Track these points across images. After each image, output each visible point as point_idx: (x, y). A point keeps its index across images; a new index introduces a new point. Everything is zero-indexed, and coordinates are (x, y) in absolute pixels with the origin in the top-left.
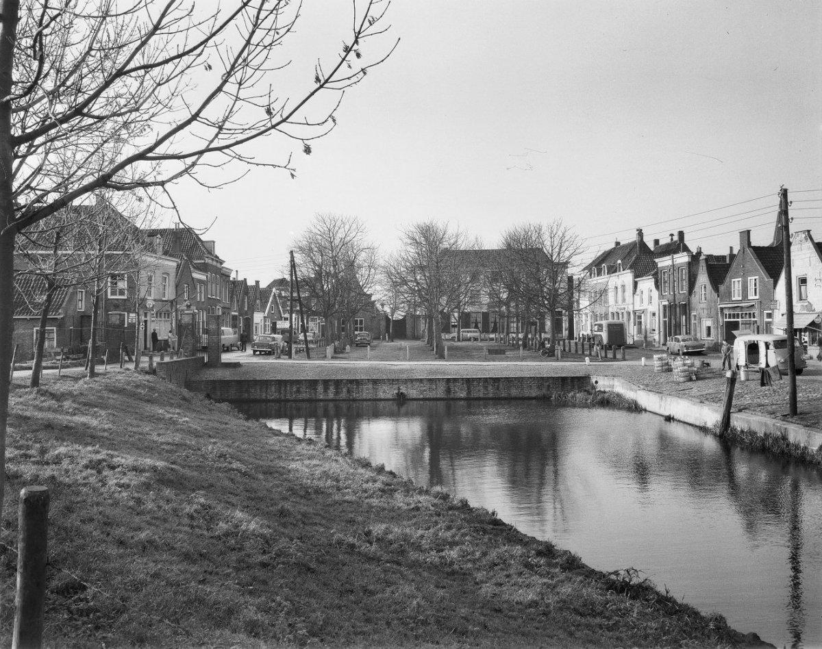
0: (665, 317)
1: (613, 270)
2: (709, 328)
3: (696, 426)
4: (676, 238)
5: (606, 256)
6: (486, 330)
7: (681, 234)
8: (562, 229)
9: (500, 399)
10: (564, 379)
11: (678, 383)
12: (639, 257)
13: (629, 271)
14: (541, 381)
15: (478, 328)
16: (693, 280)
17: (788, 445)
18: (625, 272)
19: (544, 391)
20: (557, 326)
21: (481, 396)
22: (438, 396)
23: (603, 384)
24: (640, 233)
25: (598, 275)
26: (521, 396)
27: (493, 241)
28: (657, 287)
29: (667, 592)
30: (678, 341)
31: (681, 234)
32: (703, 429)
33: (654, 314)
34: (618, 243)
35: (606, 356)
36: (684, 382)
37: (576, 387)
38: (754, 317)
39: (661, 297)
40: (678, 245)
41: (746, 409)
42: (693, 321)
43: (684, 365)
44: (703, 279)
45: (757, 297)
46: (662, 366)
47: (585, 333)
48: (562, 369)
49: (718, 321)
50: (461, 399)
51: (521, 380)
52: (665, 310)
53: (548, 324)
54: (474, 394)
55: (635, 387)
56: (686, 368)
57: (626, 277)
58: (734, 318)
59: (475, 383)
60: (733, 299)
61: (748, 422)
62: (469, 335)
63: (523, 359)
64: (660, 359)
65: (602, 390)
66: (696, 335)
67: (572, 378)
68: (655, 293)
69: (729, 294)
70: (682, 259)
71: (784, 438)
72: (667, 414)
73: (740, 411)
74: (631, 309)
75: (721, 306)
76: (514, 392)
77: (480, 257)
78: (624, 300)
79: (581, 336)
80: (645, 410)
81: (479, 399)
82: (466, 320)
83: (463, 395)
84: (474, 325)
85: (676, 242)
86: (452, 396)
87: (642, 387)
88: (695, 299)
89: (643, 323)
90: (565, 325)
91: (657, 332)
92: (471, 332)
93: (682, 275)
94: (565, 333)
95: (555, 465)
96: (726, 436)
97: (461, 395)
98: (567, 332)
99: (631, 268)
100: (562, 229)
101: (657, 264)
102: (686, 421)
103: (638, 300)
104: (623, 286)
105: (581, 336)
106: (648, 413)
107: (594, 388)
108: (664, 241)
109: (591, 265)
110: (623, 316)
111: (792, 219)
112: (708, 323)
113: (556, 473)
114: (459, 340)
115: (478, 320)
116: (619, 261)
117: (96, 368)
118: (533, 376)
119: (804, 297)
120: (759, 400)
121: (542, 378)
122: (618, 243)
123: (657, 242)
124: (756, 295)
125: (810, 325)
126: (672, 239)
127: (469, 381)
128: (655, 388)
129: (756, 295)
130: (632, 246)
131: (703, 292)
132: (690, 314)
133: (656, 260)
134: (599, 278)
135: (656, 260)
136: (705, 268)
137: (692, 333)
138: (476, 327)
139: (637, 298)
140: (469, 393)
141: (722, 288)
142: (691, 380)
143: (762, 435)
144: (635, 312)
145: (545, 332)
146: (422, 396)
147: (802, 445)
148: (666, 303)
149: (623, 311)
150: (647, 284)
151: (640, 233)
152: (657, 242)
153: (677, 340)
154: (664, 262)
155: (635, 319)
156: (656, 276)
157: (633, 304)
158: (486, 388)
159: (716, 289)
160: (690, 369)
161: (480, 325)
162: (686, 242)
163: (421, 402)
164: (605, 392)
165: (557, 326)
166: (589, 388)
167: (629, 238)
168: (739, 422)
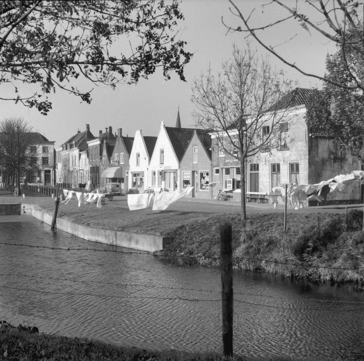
34: (79, 132)
44: (105, 153)
57: (76, 151)
101: (87, 144)
126: (107, 131)
133: (88, 142)
135: (88, 142)
150: (84, 156)
152: (101, 132)
157: (79, 166)
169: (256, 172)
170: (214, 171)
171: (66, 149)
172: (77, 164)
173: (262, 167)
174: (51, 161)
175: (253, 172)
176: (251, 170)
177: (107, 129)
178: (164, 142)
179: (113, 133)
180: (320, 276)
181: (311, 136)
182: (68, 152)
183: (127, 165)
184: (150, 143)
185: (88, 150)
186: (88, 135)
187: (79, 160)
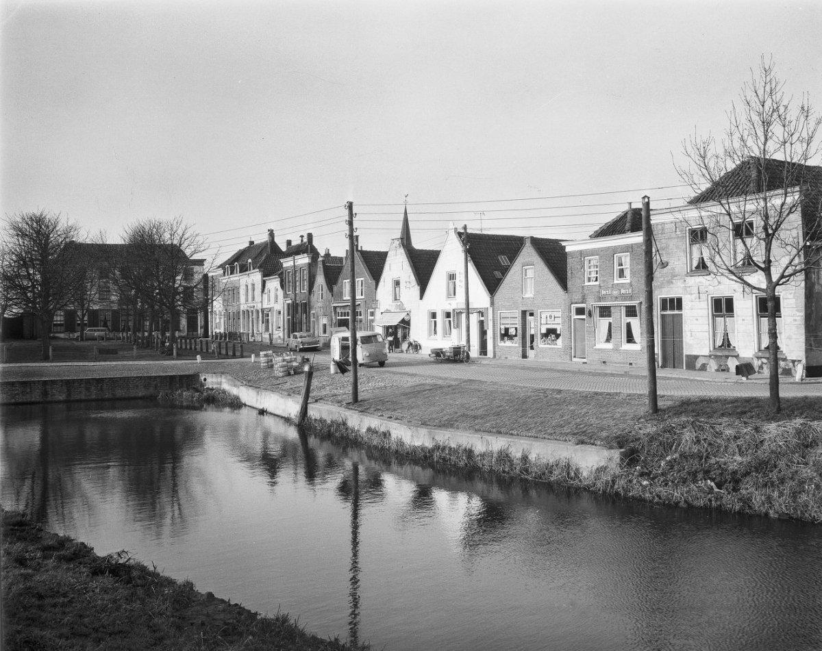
0: (288, 315)
1: (244, 269)
2: (325, 325)
3: (282, 417)
4: (305, 240)
5: (239, 256)
6: (116, 329)
7: (310, 236)
8: (183, 227)
9: (103, 400)
10: (172, 378)
11: (277, 378)
12: (265, 258)
13: (258, 270)
14: (148, 381)
15: (107, 327)
16: (312, 280)
17: (347, 429)
18: (254, 271)
19: (151, 390)
20: (192, 325)
21: (83, 397)
22: (33, 400)
23: (212, 381)
24: (271, 233)
25: (231, 274)
26: (127, 396)
27: (116, 235)
28: (282, 286)
29: (155, 568)
30: (296, 338)
31: (310, 236)
32: (287, 420)
33: (280, 313)
34: (252, 243)
35: (227, 354)
36: (283, 377)
37: (185, 385)
38: (361, 315)
39: (286, 296)
40: (307, 247)
41: (321, 399)
42: (312, 319)
43: (284, 360)
44: (320, 280)
45: (363, 297)
46: (268, 362)
47: (218, 331)
48: (172, 367)
49: (332, 320)
50: (59, 402)
51: (126, 380)
52: (288, 308)
53: (184, 322)
54: (75, 397)
55: (239, 383)
56: (285, 363)
57: (256, 276)
58: (672, 308)
59: (76, 384)
60: (345, 299)
61: (319, 411)
62: (96, 334)
63: (140, 358)
64: (266, 356)
65: (210, 387)
66: (314, 333)
67: (181, 376)
68: (280, 293)
69: (341, 294)
70: (303, 260)
71: (344, 424)
72: (261, 407)
73: (316, 401)
74: (259, 307)
75: (334, 305)
76: (120, 393)
77: (102, 252)
78: (253, 299)
79: (214, 334)
80: (245, 405)
81: (80, 401)
82: (95, 319)
83: (62, 397)
84: (102, 323)
85: (305, 243)
86: (49, 398)
87: (245, 382)
88: (314, 298)
89: (270, 321)
90: (200, 321)
91: (282, 329)
92: (98, 330)
93: (303, 275)
94: (200, 331)
95: (174, 468)
96: (304, 425)
97: (61, 398)
98: (203, 330)
99: (260, 267)
100: (183, 227)
101: (282, 264)
102: (275, 413)
103: (264, 297)
104: (253, 285)
105: (214, 334)
106: (247, 407)
107: (202, 385)
108: (296, 242)
109: (226, 263)
110: (253, 314)
111: (356, 229)
112: (324, 321)
113: (174, 476)
114: (82, 340)
115: (108, 318)
116: (250, 261)
117: (769, 394)
118: (141, 375)
119: (398, 298)
120: (335, 391)
121: (150, 378)
122: (252, 243)
123: (289, 242)
124: (362, 295)
125: (401, 322)
126: (302, 241)
127: (69, 384)
128: (254, 384)
129: (362, 295)
130: (263, 247)
131: (321, 292)
132: (309, 312)
133: (282, 260)
134: (231, 276)
135: (282, 260)
136: (322, 269)
137: (312, 332)
138: (105, 325)
139: (265, 296)
140: (69, 395)
141: (335, 288)
142: (289, 374)
143: (329, 422)
144: (263, 310)
145: (180, 331)
146: (13, 401)
147: (356, 429)
148: (290, 302)
149: (252, 309)
150: (274, 284)
151: (271, 233)
152: (289, 242)
153: (295, 337)
154: (287, 263)
155: (263, 317)
156: (281, 276)
157: (262, 302)
158: (88, 389)
159: (331, 289)
160: (289, 364)
161: (109, 324)
162: (315, 243)
163: (13, 407)
164: (212, 389)
165: (192, 325)
166: (198, 385)
167: (261, 238)
168: (314, 412)
169: (676, 312)
170: (573, 311)
171: (232, 273)
172: (258, 298)
173: (690, 304)
174: (198, 296)
175: (669, 312)
176: (664, 308)
177: (302, 236)
178: (453, 258)
179: (740, 240)
180: (28, 494)
181: (810, 247)
182: (237, 278)
183: (372, 300)
184: (423, 264)
185: (282, 273)
186: (272, 249)
187: (263, 291)
